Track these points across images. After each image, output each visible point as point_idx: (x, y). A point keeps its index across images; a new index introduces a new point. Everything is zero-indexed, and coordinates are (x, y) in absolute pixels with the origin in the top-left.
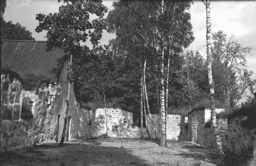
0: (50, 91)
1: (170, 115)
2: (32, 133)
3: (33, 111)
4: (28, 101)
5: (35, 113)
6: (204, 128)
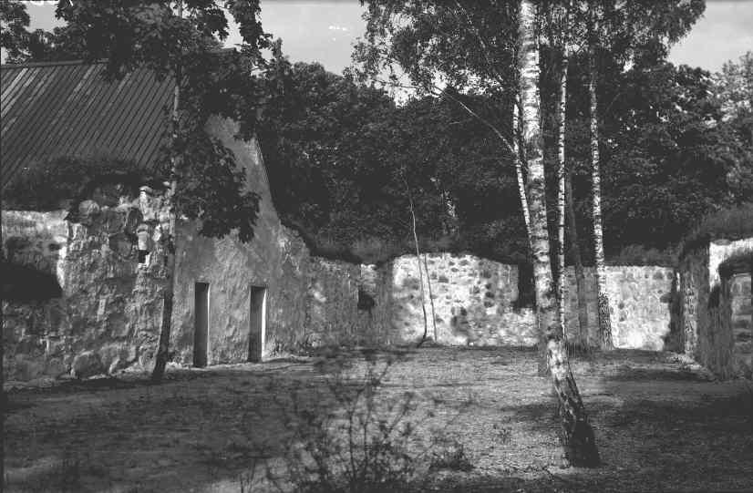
0: (145, 209)
1: (635, 267)
2: (63, 342)
3: (60, 273)
4: (46, 244)
5: (71, 278)
6: (709, 307)
